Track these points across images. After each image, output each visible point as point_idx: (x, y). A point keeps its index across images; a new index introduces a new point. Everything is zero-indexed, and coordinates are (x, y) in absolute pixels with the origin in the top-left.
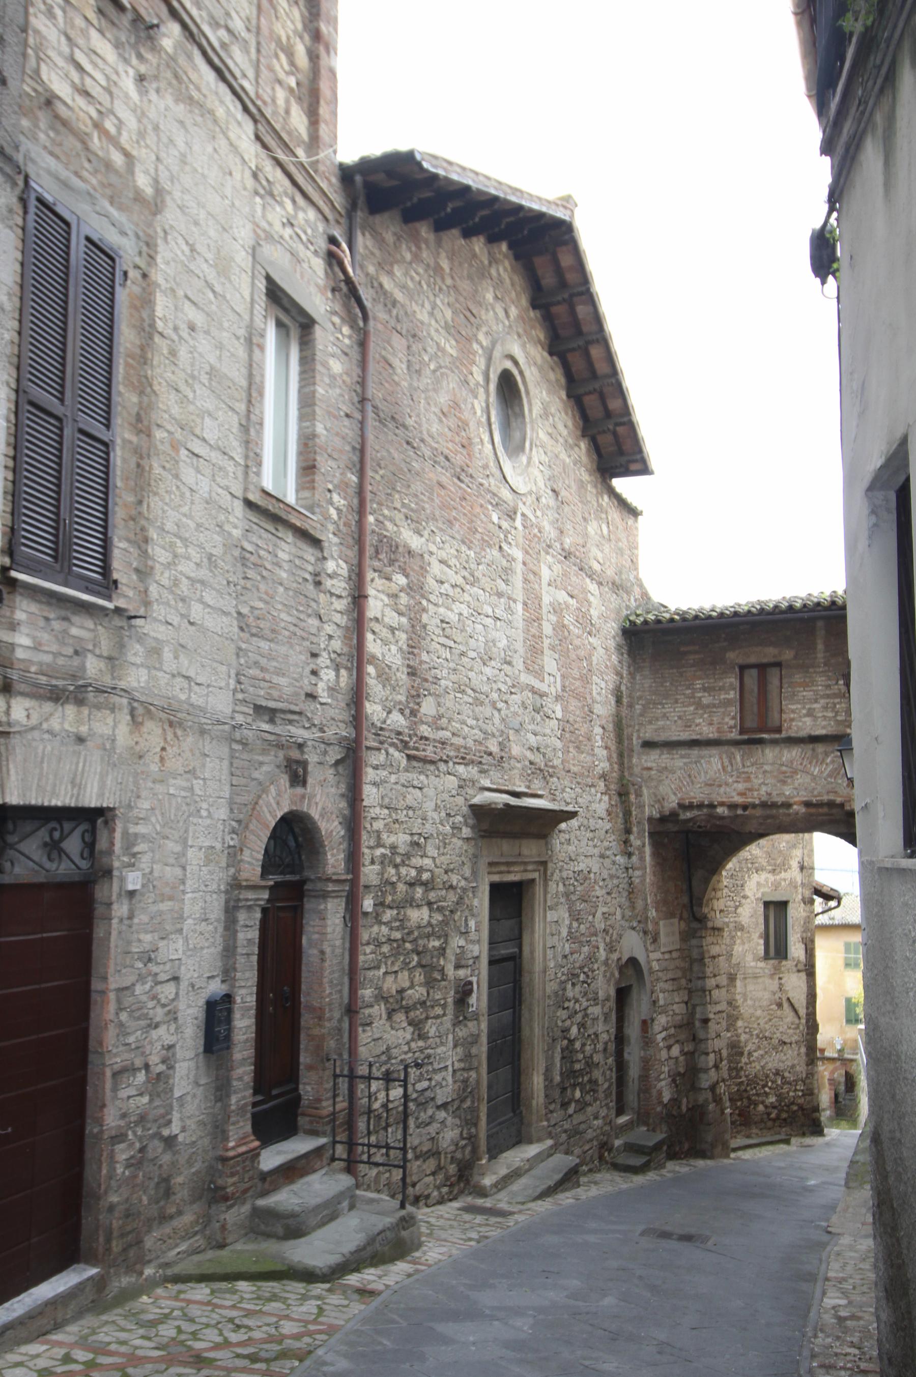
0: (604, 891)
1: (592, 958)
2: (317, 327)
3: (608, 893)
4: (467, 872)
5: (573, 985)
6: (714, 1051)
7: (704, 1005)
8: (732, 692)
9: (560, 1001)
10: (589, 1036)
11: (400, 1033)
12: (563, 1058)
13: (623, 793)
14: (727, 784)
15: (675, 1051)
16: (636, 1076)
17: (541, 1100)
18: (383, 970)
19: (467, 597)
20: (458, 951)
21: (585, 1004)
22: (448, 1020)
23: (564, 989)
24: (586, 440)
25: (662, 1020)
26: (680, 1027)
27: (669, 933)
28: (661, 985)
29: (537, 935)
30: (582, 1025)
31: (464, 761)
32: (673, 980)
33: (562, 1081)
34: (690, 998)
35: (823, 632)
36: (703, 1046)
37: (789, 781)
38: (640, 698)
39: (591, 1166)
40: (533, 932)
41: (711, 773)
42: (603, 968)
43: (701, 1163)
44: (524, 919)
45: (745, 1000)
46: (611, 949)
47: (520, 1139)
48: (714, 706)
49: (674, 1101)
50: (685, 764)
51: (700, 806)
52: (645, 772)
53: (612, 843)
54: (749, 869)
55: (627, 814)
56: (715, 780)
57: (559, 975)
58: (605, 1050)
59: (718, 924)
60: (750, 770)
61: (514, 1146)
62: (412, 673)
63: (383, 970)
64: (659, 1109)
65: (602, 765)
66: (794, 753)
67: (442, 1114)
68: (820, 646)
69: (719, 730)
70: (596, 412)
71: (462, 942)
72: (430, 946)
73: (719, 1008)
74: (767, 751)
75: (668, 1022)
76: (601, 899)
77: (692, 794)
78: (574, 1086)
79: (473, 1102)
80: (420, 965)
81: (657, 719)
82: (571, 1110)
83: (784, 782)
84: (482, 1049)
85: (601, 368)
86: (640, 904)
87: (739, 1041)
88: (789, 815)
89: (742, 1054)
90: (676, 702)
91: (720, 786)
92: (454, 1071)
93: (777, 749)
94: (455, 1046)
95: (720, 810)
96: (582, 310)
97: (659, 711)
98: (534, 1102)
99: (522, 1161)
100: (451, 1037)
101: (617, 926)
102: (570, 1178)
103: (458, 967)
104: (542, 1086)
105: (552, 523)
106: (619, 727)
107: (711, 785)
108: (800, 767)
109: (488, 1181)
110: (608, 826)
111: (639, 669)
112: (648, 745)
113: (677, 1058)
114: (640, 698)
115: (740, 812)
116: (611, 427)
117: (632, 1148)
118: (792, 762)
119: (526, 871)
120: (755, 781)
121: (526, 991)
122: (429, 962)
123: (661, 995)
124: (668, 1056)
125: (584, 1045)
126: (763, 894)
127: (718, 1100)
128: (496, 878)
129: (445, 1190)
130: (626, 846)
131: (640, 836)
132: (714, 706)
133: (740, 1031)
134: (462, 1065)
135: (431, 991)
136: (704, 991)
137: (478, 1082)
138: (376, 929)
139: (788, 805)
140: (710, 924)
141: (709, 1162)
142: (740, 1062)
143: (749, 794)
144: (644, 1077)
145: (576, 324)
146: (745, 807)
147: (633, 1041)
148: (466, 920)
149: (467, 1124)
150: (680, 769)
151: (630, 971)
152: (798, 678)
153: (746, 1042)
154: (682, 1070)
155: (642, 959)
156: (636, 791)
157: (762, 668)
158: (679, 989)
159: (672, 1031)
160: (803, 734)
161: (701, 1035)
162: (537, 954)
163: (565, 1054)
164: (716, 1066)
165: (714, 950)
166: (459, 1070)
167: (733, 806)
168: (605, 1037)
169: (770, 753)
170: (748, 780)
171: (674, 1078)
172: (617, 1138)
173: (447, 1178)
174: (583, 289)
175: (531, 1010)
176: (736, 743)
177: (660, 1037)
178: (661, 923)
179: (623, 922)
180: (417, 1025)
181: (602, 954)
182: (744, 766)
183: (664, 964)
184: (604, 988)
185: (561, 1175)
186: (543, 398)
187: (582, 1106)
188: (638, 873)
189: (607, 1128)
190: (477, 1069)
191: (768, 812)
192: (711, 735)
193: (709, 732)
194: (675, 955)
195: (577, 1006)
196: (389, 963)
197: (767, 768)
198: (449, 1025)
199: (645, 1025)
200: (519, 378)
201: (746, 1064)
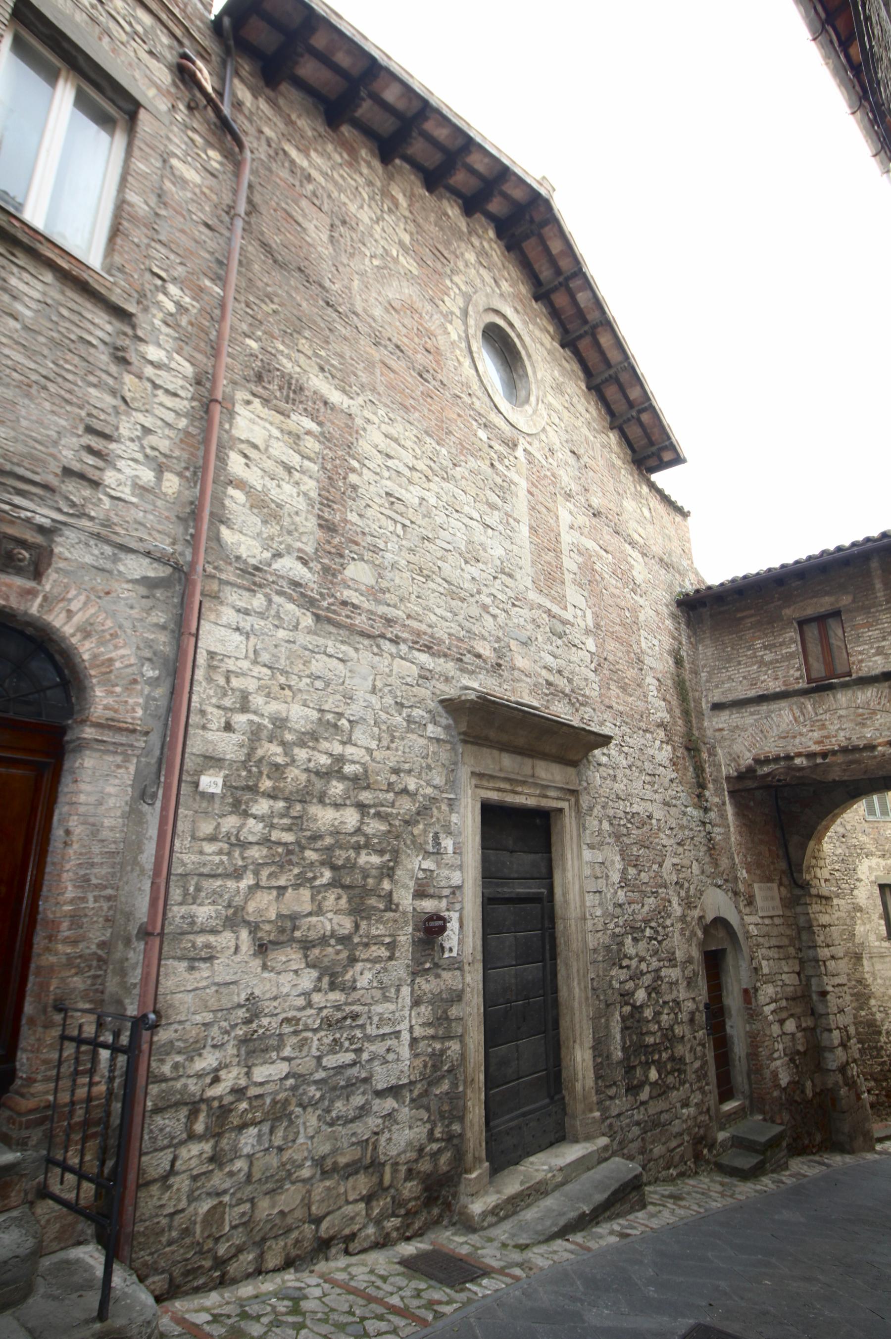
0: (672, 841)
1: (662, 911)
2: (142, 112)
3: (679, 844)
4: (438, 780)
5: (635, 940)
6: (838, 1028)
7: (819, 976)
8: (793, 646)
9: (614, 956)
10: (665, 1003)
12: (625, 1029)
13: (692, 749)
14: (801, 734)
15: (790, 1026)
16: (743, 1055)
17: (590, 1082)
19: (432, 485)
20: (421, 875)
21: (655, 964)
22: (400, 968)
23: (621, 944)
24: (616, 432)
25: (768, 991)
26: (794, 999)
27: (767, 898)
28: (761, 952)
29: (569, 875)
30: (652, 990)
32: (778, 947)
33: (627, 1058)
34: (802, 968)
35: (879, 572)
36: (824, 1021)
37: (868, 722)
38: (704, 666)
39: (682, 1168)
40: (564, 870)
41: (784, 726)
42: (679, 925)
43: (837, 1160)
44: (554, 855)
45: (875, 979)
46: (689, 904)
47: (560, 1136)
48: (777, 661)
49: (796, 1085)
50: (755, 720)
51: (777, 759)
52: (717, 734)
53: (682, 794)
54: (859, 854)
55: (699, 769)
56: (792, 732)
57: (612, 926)
58: (692, 1021)
59: (825, 889)
60: (823, 717)
61: (551, 1144)
62: (328, 527)
63: (248, 880)
64: (776, 1094)
65: (659, 714)
66: (869, 694)
67: (390, 1103)
68: (878, 585)
69: (785, 683)
70: (620, 406)
71: (428, 864)
73: (837, 980)
74: (839, 696)
75: (777, 993)
76: (669, 849)
77: (767, 749)
78: (647, 1065)
79: (454, 1085)
80: (334, 883)
81: (723, 683)
82: (644, 1095)
83: (863, 725)
84: (471, 1011)
85: (614, 356)
86: (724, 862)
87: (875, 1020)
88: (875, 757)
89: (879, 1033)
90: (739, 663)
91: (795, 737)
92: (414, 1041)
93: (850, 693)
94: (416, 1003)
95: (798, 761)
96: (582, 297)
97: (724, 675)
98: (579, 1086)
99: (551, 1170)
100: (406, 991)
101: (695, 880)
102: (625, 1197)
103: (420, 894)
104: (590, 1064)
105: (574, 478)
106: (681, 688)
107: (785, 738)
108: (878, 707)
109: (477, 1207)
110: (674, 775)
111: (700, 641)
112: (717, 707)
113: (793, 1034)
114: (704, 666)
115: (819, 760)
116: (634, 414)
117: (740, 1143)
118: (868, 703)
119: (546, 797)
120: (831, 727)
121: (561, 940)
122: (360, 882)
123: (764, 963)
124: (781, 1033)
125: (657, 1014)
126: (877, 877)
127: (851, 1084)
128: (494, 796)
129: (395, 1222)
130: (700, 801)
131: (718, 792)
132: (777, 661)
133: (874, 1010)
134: (431, 1031)
135: (363, 924)
136: (817, 961)
137: (463, 1056)
139: (871, 747)
140: (813, 891)
141: (848, 1159)
142: (879, 1041)
143: (827, 741)
144: (753, 1055)
145: (580, 314)
146: (824, 755)
147: (734, 1012)
148: (436, 837)
149: (442, 1118)
150: (752, 725)
151: (721, 934)
152: (860, 619)
153: (883, 1021)
154: (801, 1048)
155: (733, 919)
156: (708, 750)
157: (821, 620)
158: (787, 958)
159: (784, 1003)
160: (877, 671)
161: (820, 1009)
162: (571, 896)
163: (628, 1023)
164: (843, 1045)
165: (824, 919)
166: (424, 1038)
167: (811, 756)
168: (689, 1005)
169: (843, 697)
170: (823, 727)
171: (793, 1056)
172: (722, 1128)
173: (398, 1203)
174: (646, 405)
175: (568, 966)
176: (804, 693)
177: (768, 1009)
178: (756, 886)
179: (703, 877)
181: (677, 909)
182: (816, 714)
183: (766, 929)
184: (684, 947)
185: (606, 1195)
186: (535, 338)
187: (661, 1090)
188: (717, 830)
189: (704, 1118)
190: (461, 1038)
191: (851, 757)
192: (778, 690)
193: (775, 686)
194: (777, 921)
195: (643, 966)
196: (265, 873)
197: (842, 712)
198: (403, 973)
199: (748, 995)
201: (885, 1043)
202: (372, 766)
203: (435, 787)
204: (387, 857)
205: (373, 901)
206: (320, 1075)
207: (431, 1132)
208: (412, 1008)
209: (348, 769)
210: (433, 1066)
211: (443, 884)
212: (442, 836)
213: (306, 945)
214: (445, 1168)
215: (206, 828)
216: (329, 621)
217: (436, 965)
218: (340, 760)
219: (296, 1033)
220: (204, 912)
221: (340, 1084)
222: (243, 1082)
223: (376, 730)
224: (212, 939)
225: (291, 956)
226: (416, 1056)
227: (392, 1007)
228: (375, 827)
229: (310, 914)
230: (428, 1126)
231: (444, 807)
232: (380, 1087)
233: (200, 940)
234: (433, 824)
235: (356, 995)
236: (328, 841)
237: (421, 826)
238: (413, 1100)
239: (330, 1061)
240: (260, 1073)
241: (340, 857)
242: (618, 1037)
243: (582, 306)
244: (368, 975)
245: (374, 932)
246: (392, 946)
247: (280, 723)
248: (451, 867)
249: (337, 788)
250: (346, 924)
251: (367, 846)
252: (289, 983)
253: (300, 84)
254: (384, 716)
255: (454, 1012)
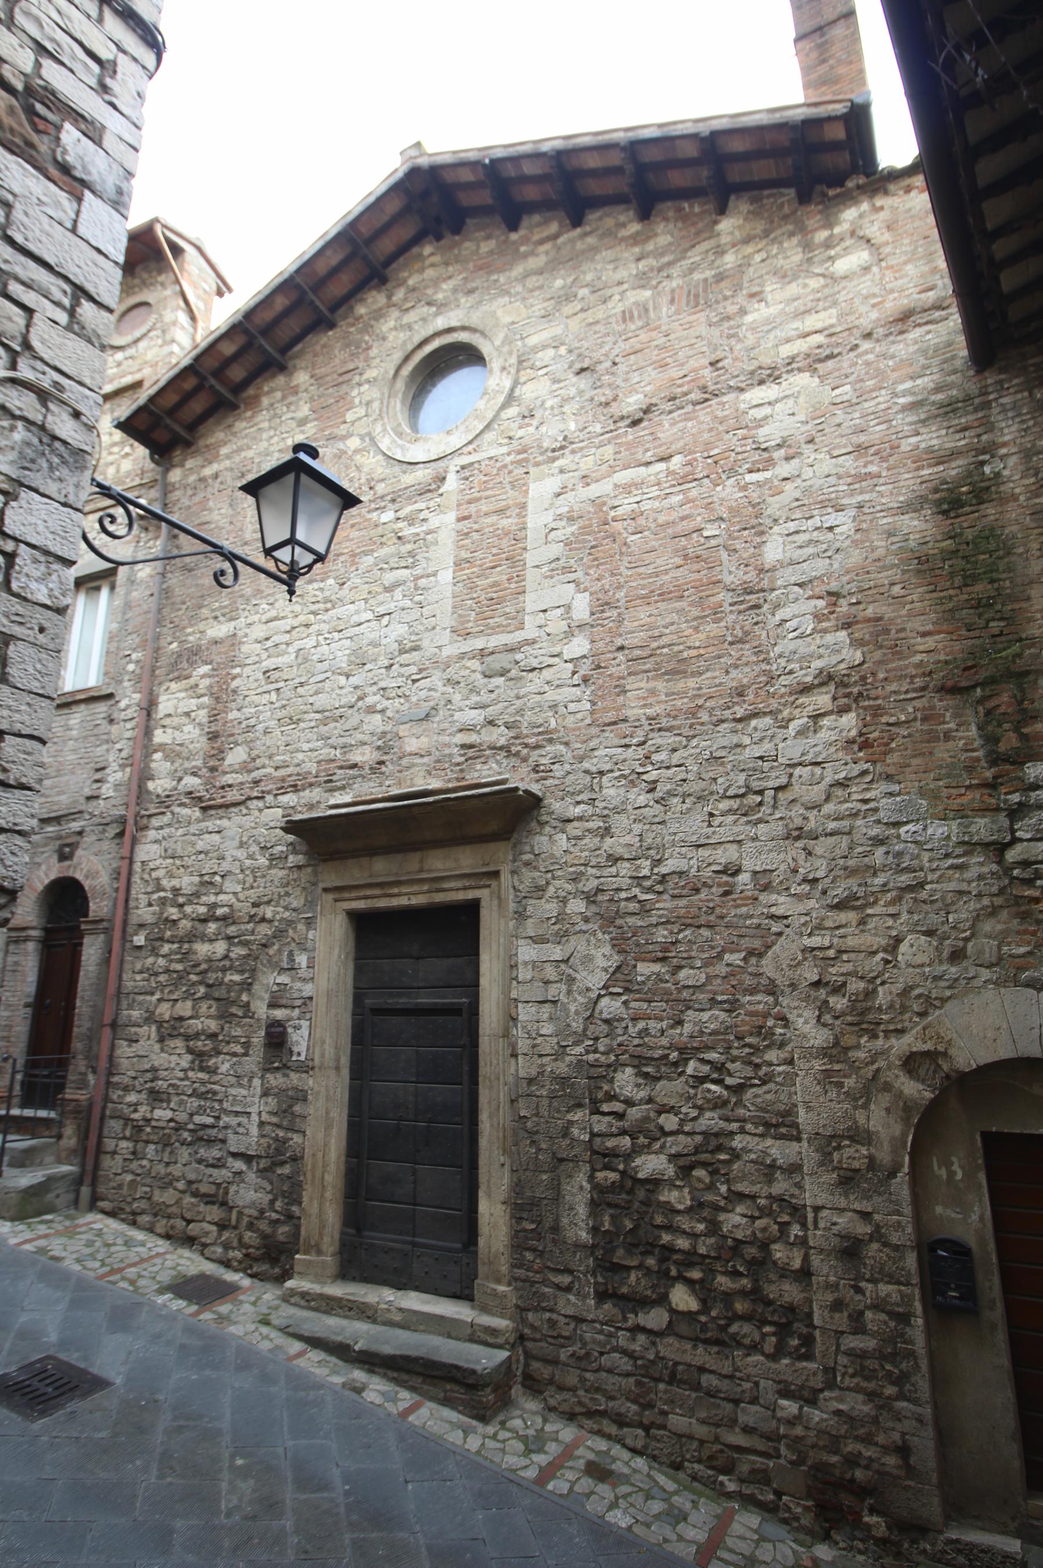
11: (174, 1058)
18: (157, 996)
22: (252, 1063)
31: (282, 791)
63: (157, 996)
72: (226, 980)
80: (206, 997)
92: (262, 1124)
94: (265, 1094)
103: (272, 1005)
122: (225, 996)
134: (274, 1120)
138: (151, 960)
148: (291, 954)
180: (200, 1058)
196: (166, 991)
200: (428, 349)
202: (238, 905)
203: (294, 910)
204: (246, 975)
205: (234, 1010)
206: (191, 1126)
207: (272, 1202)
208: (261, 1097)
209: (220, 912)
210: (276, 1149)
211: (295, 996)
212: (296, 953)
213: (187, 1038)
214: (282, 1238)
215: (138, 966)
216: (211, 807)
217: (285, 1066)
218: (214, 906)
219: (178, 1094)
220: (136, 1014)
221: (202, 1137)
222: (148, 1116)
223: (241, 876)
224: (137, 1029)
225: (179, 1043)
226: (263, 1136)
227: (244, 1092)
228: (239, 951)
229: (190, 1018)
230: (270, 1197)
231: (301, 927)
232: (232, 1149)
233: (133, 1029)
234: (289, 943)
235: (216, 1078)
236: (204, 966)
237: (276, 947)
238: (259, 1171)
239: (197, 1119)
240: (158, 1113)
241: (211, 978)
242: (582, 1211)
243: (540, 172)
244: (227, 1065)
245: (234, 1034)
246: (247, 1045)
247: (176, 891)
248: (304, 980)
249: (212, 927)
250: (213, 1025)
251: (231, 968)
252: (174, 1060)
253: (246, 383)
254: (248, 862)
255: (297, 1108)
